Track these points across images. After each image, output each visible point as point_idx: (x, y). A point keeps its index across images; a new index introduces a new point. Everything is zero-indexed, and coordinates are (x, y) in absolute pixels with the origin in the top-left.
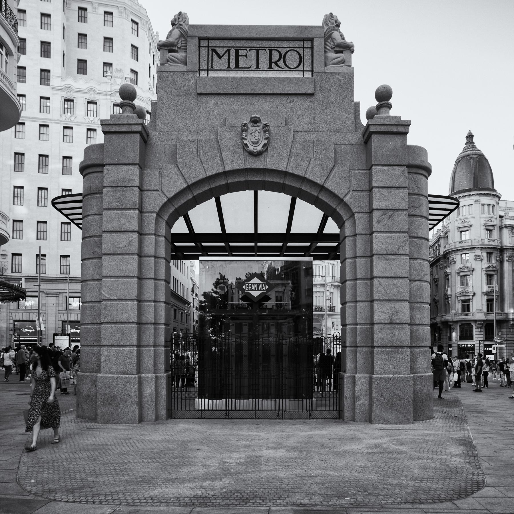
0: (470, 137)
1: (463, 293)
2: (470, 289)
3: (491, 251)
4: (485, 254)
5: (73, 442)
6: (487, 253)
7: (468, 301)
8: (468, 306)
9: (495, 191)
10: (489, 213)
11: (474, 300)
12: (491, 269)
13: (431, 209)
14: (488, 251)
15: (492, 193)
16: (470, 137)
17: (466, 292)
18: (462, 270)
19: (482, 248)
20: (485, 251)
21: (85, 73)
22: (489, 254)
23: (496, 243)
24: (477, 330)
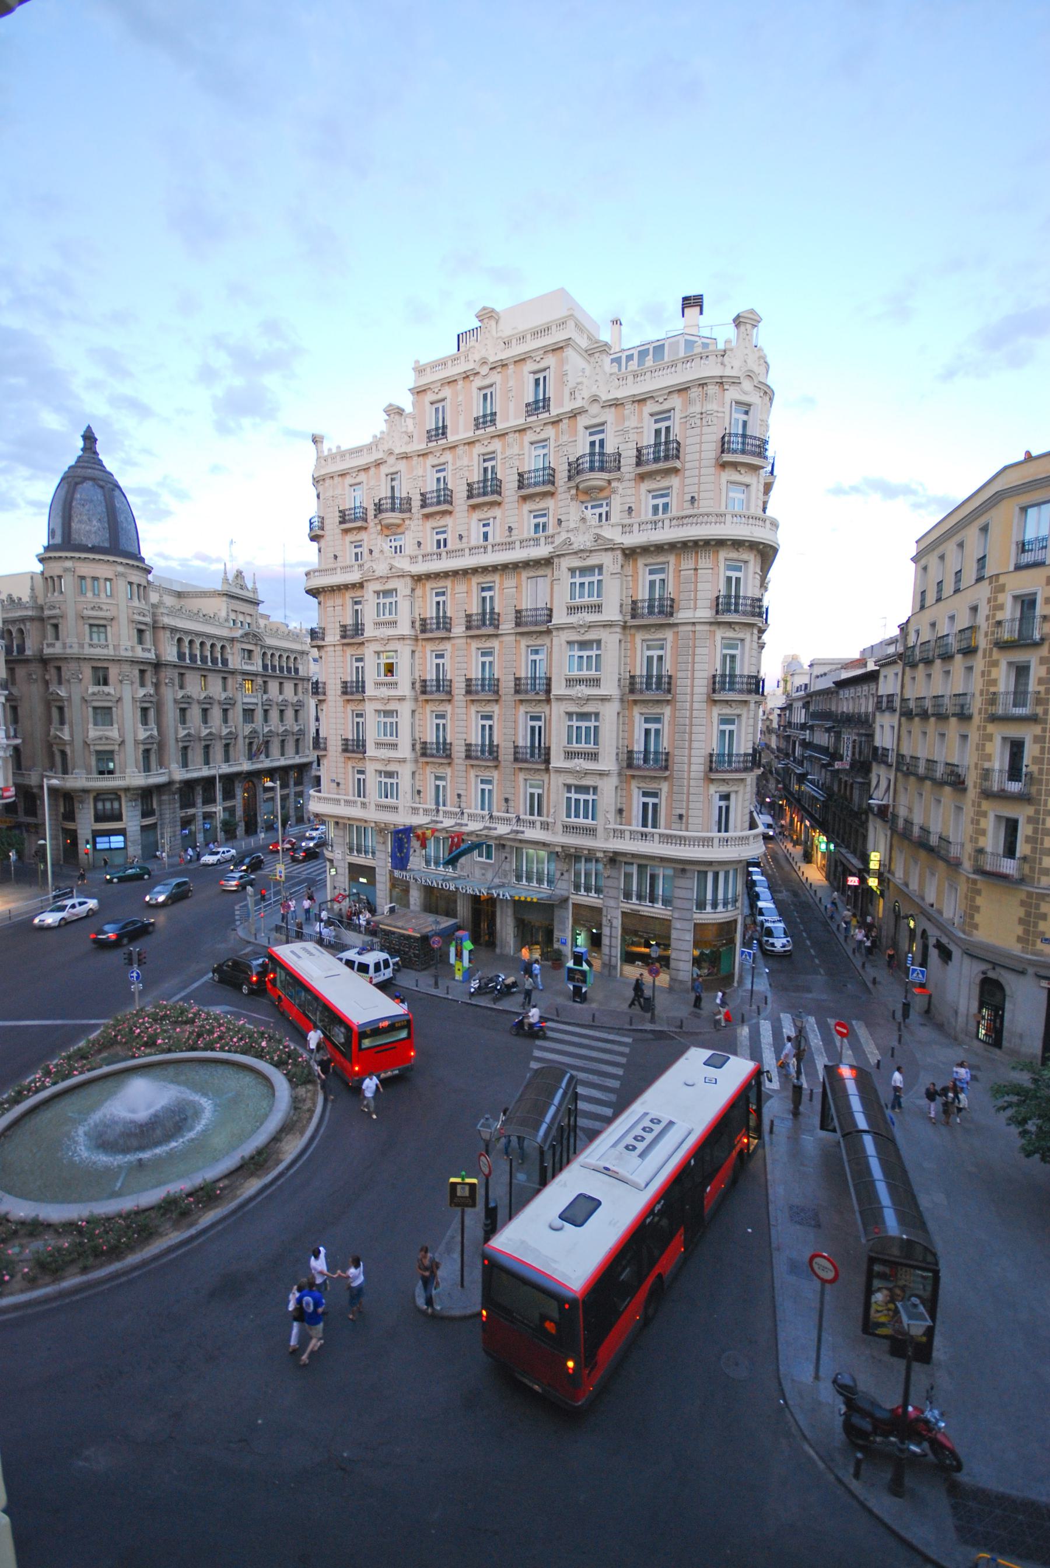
1: (101, 739)
9: (142, 560)
12: (147, 699)
15: (136, 563)
16: (89, 438)
17: (107, 738)
23: (152, 656)
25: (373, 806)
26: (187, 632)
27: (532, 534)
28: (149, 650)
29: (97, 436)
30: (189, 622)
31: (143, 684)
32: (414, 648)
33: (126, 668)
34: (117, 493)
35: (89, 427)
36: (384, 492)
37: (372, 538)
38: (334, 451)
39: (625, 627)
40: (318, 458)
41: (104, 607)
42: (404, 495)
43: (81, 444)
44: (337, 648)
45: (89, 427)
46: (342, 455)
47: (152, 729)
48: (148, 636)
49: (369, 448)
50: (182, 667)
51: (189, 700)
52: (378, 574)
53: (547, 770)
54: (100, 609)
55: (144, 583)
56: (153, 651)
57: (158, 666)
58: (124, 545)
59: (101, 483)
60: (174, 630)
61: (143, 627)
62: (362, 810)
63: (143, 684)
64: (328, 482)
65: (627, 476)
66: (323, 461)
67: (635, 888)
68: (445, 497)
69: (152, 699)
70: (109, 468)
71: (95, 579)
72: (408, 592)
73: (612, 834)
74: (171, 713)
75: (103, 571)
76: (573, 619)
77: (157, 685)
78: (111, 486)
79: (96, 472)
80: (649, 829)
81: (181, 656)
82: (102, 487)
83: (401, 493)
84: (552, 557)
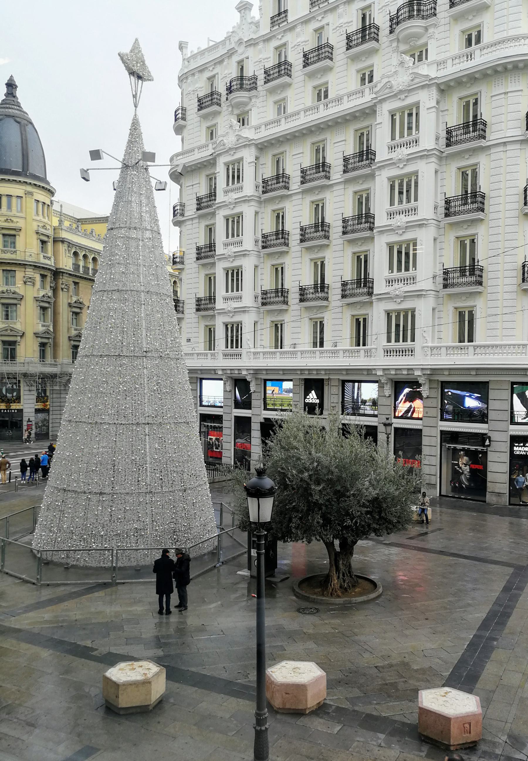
0: (11, 86)
1: (6, 330)
2: (18, 326)
3: (46, 274)
4: (38, 278)
5: (271, 240)
6: (41, 274)
7: (14, 343)
8: (13, 351)
9: (48, 183)
10: (37, 214)
11: (22, 344)
12: (45, 299)
13: (233, 221)
14: (42, 273)
15: (42, 185)
16: (11, 86)
17: (11, 330)
18: (5, 295)
19: (36, 267)
20: (38, 272)
21: (154, 154)
22: (43, 276)
23: (50, 263)
24: (27, 388)
25: (221, 356)
26: (81, 247)
27: (359, 86)
28: (49, 258)
29: (17, 84)
30: (84, 239)
31: (43, 287)
32: (258, 209)
33: (30, 273)
34: (29, 128)
35: (12, 76)
36: (234, 73)
37: (226, 121)
38: (196, 52)
39: (440, 158)
40: (184, 60)
41: (15, 220)
42: (250, 74)
43: (4, 90)
44: (194, 221)
45: (12, 76)
46: (202, 53)
47: (49, 326)
48: (50, 245)
49: (223, 43)
50: (76, 276)
51: (81, 306)
52: (228, 146)
53: (370, 294)
54: (12, 221)
55: (48, 202)
56: (52, 259)
57: (57, 273)
58: (34, 169)
59: (18, 119)
60: (70, 244)
61: (45, 239)
62: (213, 361)
63: (43, 287)
64: (190, 79)
65: (443, 22)
66: (186, 62)
67: (363, 277)
68: (283, 68)
69: (49, 300)
70: (25, 109)
71: (9, 196)
72: (253, 159)
73: (429, 353)
74: (64, 314)
75: (16, 190)
76: (395, 155)
77: (55, 290)
78: (26, 122)
79: (16, 112)
80: (466, 343)
81: (76, 267)
82: (19, 123)
83: (249, 73)
84: (375, 105)
